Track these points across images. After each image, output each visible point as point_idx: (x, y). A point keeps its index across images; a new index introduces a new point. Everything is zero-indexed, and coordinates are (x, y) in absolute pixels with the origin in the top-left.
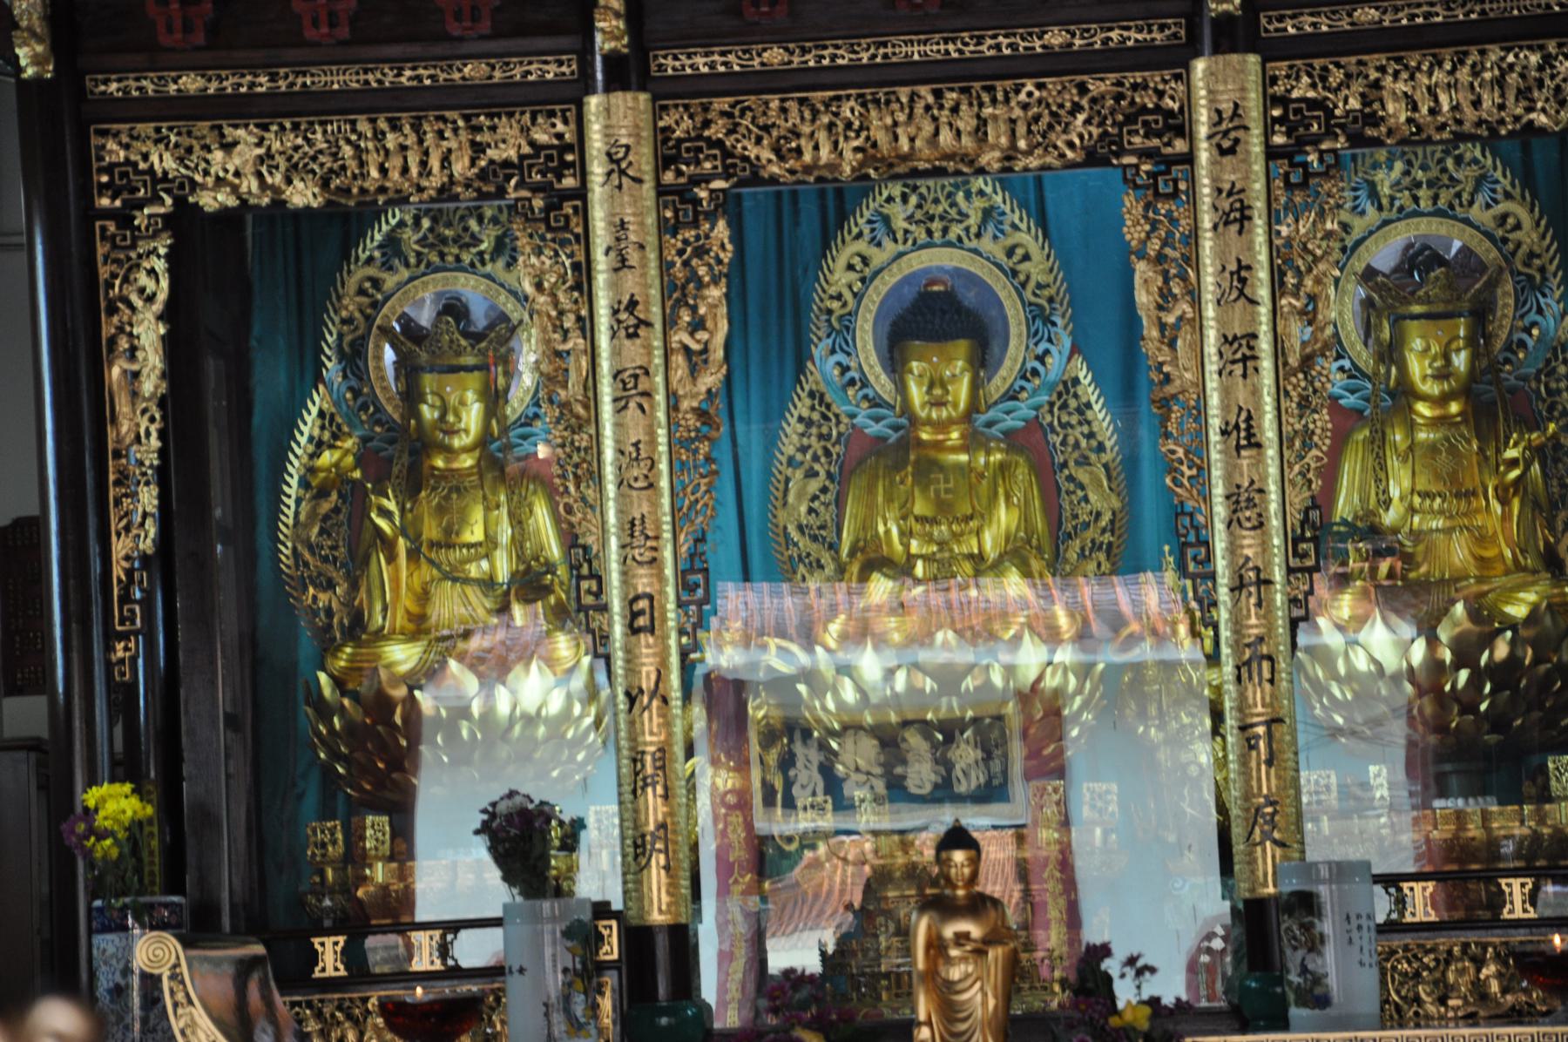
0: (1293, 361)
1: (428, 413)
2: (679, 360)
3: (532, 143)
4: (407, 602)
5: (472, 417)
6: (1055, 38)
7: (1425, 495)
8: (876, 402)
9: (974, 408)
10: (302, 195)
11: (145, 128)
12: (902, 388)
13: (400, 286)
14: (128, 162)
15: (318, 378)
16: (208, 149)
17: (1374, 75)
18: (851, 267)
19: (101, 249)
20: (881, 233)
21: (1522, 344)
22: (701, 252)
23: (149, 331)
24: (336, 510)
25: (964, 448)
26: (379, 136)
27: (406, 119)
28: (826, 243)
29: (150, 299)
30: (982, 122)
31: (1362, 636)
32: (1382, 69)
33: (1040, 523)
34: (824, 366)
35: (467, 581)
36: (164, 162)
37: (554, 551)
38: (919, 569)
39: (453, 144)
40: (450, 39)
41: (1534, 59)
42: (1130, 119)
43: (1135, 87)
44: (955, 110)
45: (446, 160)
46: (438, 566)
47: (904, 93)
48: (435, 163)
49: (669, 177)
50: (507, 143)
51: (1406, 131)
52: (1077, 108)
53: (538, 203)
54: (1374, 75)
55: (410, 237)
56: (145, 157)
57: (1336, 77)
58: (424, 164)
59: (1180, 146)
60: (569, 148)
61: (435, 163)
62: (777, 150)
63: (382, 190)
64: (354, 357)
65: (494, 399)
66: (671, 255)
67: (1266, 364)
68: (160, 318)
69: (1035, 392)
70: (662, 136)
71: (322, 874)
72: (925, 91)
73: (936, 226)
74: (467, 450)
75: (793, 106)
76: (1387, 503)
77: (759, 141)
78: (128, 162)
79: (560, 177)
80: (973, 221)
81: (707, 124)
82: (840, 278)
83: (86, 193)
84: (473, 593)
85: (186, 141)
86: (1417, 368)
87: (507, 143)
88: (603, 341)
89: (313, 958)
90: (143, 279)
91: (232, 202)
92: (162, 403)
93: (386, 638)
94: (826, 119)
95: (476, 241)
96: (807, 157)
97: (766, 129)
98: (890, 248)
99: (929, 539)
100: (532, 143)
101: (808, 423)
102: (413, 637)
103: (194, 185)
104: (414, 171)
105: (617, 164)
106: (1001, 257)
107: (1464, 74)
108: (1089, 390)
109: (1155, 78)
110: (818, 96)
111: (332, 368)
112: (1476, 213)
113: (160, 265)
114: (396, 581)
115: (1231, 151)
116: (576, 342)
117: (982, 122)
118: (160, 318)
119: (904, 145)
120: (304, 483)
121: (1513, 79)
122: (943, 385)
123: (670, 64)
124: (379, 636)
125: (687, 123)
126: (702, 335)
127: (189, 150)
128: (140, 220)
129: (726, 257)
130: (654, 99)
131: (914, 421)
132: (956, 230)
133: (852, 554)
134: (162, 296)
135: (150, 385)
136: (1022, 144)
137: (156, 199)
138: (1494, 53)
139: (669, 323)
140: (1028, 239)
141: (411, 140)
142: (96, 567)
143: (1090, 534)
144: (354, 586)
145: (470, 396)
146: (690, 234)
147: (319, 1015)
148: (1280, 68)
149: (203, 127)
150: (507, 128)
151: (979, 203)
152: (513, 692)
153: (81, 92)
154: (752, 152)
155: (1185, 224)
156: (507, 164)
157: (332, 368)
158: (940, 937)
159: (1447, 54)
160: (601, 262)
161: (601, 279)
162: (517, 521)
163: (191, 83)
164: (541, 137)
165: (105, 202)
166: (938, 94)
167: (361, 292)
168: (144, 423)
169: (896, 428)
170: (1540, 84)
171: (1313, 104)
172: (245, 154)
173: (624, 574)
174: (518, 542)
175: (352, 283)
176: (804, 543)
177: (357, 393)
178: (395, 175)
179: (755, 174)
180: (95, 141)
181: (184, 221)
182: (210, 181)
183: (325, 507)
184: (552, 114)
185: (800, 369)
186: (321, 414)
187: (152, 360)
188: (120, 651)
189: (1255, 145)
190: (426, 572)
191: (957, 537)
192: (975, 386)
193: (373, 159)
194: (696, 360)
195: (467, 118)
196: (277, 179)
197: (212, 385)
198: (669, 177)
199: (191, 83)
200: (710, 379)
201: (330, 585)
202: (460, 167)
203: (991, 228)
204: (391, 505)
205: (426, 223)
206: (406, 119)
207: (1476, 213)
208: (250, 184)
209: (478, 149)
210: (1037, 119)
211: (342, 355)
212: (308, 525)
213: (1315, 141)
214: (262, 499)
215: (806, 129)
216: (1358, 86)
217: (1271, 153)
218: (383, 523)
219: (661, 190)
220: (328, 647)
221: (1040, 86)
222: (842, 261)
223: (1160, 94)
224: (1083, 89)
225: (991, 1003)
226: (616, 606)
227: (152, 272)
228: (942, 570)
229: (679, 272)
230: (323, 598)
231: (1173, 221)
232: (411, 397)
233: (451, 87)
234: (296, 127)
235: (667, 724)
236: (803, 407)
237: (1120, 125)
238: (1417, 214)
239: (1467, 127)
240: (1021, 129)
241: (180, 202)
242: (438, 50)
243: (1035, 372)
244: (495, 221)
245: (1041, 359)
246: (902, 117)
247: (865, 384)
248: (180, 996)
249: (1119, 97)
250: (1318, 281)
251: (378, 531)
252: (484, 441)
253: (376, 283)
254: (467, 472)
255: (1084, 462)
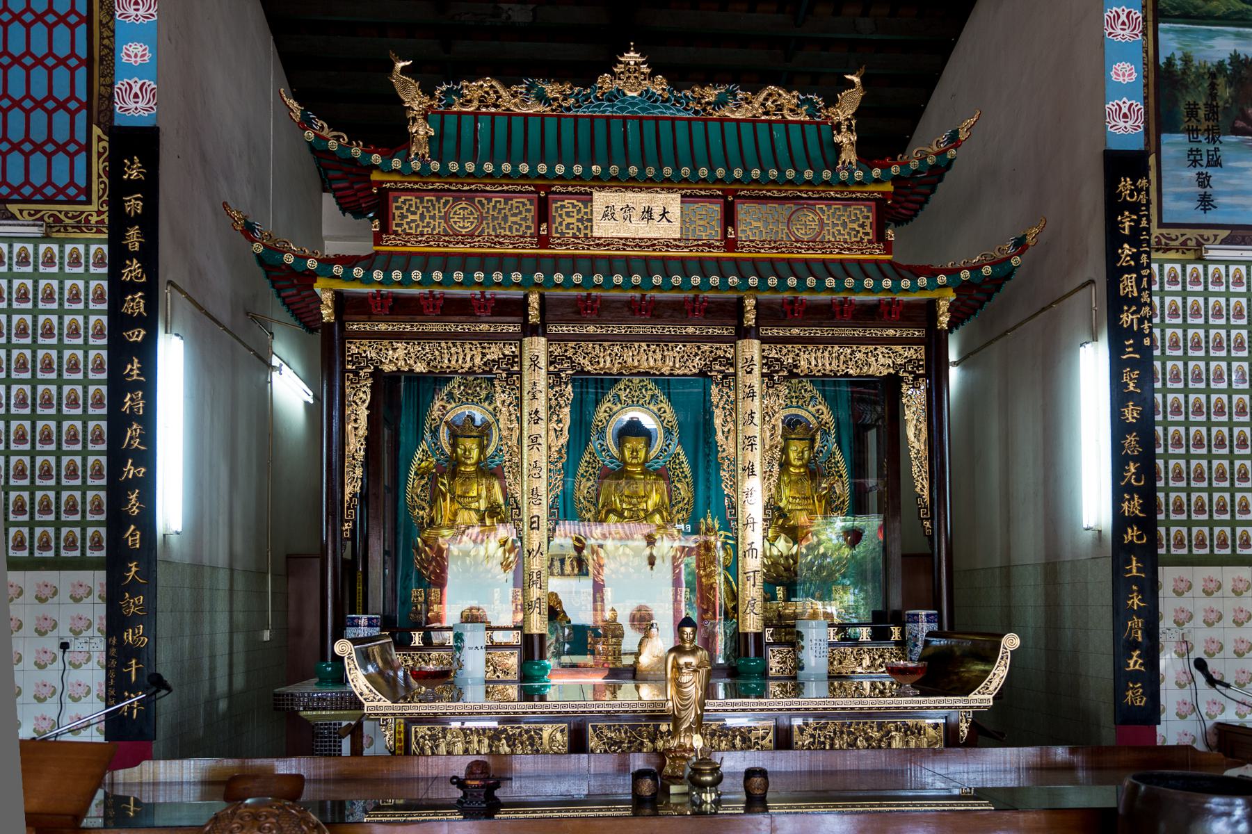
0: (767, 447)
1: (460, 451)
2: (552, 433)
3: (503, 354)
4: (449, 515)
5: (475, 454)
6: (690, 330)
7: (794, 498)
8: (612, 457)
9: (646, 461)
10: (420, 368)
11: (365, 342)
12: (622, 452)
13: (452, 409)
14: (359, 353)
15: (423, 438)
16: (387, 350)
17: (797, 351)
18: (605, 411)
19: (347, 383)
20: (617, 400)
21: (821, 451)
22: (562, 395)
23: (363, 413)
24: (427, 483)
25: (642, 474)
26: (449, 348)
27: (458, 343)
28: (597, 403)
29: (364, 402)
30: (664, 357)
31: (776, 543)
32: (800, 350)
33: (667, 500)
34: (594, 444)
35: (470, 509)
36: (371, 354)
37: (501, 501)
38: (626, 514)
39: (475, 352)
40: (475, 315)
41: (849, 351)
42: (715, 359)
43: (717, 349)
44: (654, 352)
45: (472, 359)
46: (460, 504)
47: (636, 345)
48: (468, 359)
49: (552, 369)
50: (494, 352)
51: (807, 371)
52: (697, 354)
53: (504, 375)
54: (797, 351)
55: (457, 392)
56: (365, 352)
57: (785, 351)
58: (464, 359)
59: (732, 370)
60: (517, 356)
61: (468, 359)
62: (591, 362)
63: (448, 367)
64: (435, 432)
65: (483, 448)
66: (551, 396)
67: (758, 446)
68: (367, 408)
69: (665, 457)
70: (550, 354)
71: (416, 606)
72: (644, 344)
73: (635, 399)
74: (472, 465)
75: (597, 346)
76: (781, 500)
77: (584, 358)
78: (359, 353)
79: (513, 367)
80: (647, 399)
81: (566, 351)
82: (601, 414)
83: (343, 364)
84: (473, 514)
85: (380, 347)
86: (793, 455)
87: (494, 352)
88: (525, 424)
89: (411, 639)
90: (361, 395)
91: (395, 369)
92: (366, 439)
93: (442, 527)
94: (609, 352)
95: (479, 395)
96: (601, 365)
97: (587, 354)
98: (619, 406)
99: (630, 503)
100: (503, 354)
101: (589, 463)
102: (451, 528)
103: (381, 362)
104: (460, 362)
105: (534, 362)
106: (656, 411)
107: (827, 354)
108: (682, 457)
109: (724, 346)
110: (606, 344)
111: (428, 435)
112: (810, 408)
113: (368, 391)
114: (446, 507)
115: (750, 372)
116: (516, 425)
117: (664, 357)
118: (367, 408)
119: (636, 363)
120: (416, 474)
121: (842, 357)
122: (637, 452)
123: (553, 329)
124: (440, 527)
125: (559, 350)
126: (561, 425)
127: (381, 350)
128: (362, 373)
129: (571, 398)
130: (548, 341)
131: (625, 463)
132: (641, 401)
133: (603, 507)
134: (368, 402)
135: (362, 432)
136: (677, 365)
137: (367, 366)
138: (836, 348)
139: (549, 420)
140: (665, 406)
141: (460, 350)
142: (339, 496)
143: (680, 505)
144: (431, 509)
145: (474, 446)
146: (558, 389)
147: (413, 659)
148: (766, 346)
149: (386, 342)
150: (494, 348)
151: (650, 393)
152: (486, 549)
153: (342, 328)
154: (582, 361)
155: (732, 398)
156: (493, 361)
157: (428, 435)
158: (678, 664)
159: (821, 346)
160: (526, 397)
161: (525, 402)
162: (489, 490)
163: (383, 327)
164: (507, 353)
165: (350, 367)
166: (648, 346)
167: (439, 410)
168: (359, 445)
169: (618, 466)
170: (851, 359)
171: (777, 360)
172: (401, 353)
173: (529, 508)
174: (488, 498)
175: (436, 407)
176: (585, 503)
177: (436, 444)
178: (453, 362)
179: (582, 369)
180: (348, 345)
181: (377, 374)
182: (387, 361)
183: (423, 482)
184: (511, 344)
185: (587, 444)
186: (423, 451)
187: (363, 423)
188: (346, 527)
189: (756, 371)
190: (456, 506)
191: (639, 503)
192: (647, 453)
193: (446, 357)
194: (558, 433)
195: (480, 344)
196: (412, 362)
197: (386, 438)
198: (552, 369)
199: (383, 327)
200: (563, 440)
201: (424, 509)
202: (477, 361)
203: (653, 402)
204: (446, 482)
205: (462, 388)
206: (458, 343)
207: (810, 408)
208: (401, 363)
209: (484, 355)
210: (683, 357)
211: (431, 431)
212: (417, 488)
213: (777, 372)
214: (402, 478)
215: (602, 355)
216: (791, 355)
217: (763, 375)
218: (442, 488)
219: (549, 373)
220: (422, 529)
221: (684, 346)
222: (603, 409)
223: (726, 352)
224: (699, 348)
225: (700, 692)
226: (525, 519)
227: (364, 392)
228: (634, 518)
229: (553, 403)
230: (421, 513)
231: (729, 397)
232: (454, 446)
233: (475, 334)
234: (419, 344)
235: (1218, 804)
236: (587, 457)
237: (711, 362)
238: (791, 407)
239: (827, 372)
240: (677, 360)
241: (376, 368)
242: (471, 319)
243: (665, 450)
244: (486, 388)
245: (668, 446)
246: (635, 353)
247: (608, 451)
248: (352, 666)
249: (711, 352)
250: (776, 420)
251: (440, 489)
252: (478, 462)
253: (444, 407)
254: (470, 473)
255: (680, 481)
